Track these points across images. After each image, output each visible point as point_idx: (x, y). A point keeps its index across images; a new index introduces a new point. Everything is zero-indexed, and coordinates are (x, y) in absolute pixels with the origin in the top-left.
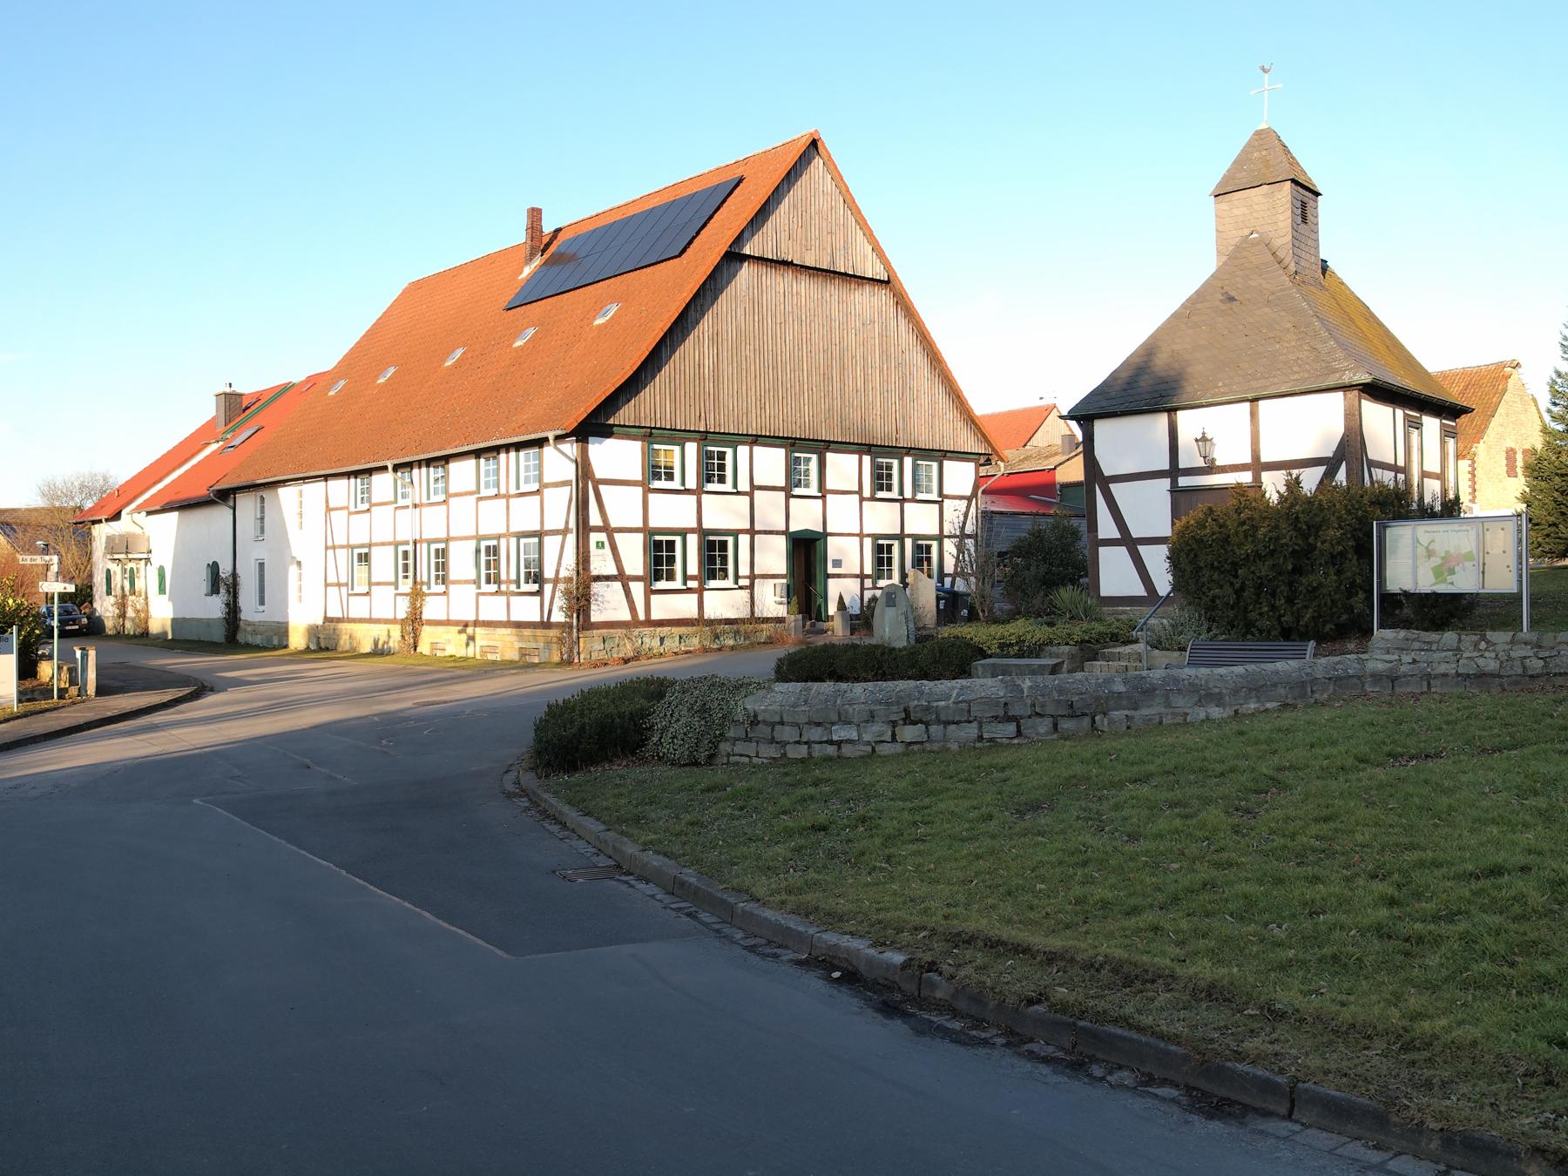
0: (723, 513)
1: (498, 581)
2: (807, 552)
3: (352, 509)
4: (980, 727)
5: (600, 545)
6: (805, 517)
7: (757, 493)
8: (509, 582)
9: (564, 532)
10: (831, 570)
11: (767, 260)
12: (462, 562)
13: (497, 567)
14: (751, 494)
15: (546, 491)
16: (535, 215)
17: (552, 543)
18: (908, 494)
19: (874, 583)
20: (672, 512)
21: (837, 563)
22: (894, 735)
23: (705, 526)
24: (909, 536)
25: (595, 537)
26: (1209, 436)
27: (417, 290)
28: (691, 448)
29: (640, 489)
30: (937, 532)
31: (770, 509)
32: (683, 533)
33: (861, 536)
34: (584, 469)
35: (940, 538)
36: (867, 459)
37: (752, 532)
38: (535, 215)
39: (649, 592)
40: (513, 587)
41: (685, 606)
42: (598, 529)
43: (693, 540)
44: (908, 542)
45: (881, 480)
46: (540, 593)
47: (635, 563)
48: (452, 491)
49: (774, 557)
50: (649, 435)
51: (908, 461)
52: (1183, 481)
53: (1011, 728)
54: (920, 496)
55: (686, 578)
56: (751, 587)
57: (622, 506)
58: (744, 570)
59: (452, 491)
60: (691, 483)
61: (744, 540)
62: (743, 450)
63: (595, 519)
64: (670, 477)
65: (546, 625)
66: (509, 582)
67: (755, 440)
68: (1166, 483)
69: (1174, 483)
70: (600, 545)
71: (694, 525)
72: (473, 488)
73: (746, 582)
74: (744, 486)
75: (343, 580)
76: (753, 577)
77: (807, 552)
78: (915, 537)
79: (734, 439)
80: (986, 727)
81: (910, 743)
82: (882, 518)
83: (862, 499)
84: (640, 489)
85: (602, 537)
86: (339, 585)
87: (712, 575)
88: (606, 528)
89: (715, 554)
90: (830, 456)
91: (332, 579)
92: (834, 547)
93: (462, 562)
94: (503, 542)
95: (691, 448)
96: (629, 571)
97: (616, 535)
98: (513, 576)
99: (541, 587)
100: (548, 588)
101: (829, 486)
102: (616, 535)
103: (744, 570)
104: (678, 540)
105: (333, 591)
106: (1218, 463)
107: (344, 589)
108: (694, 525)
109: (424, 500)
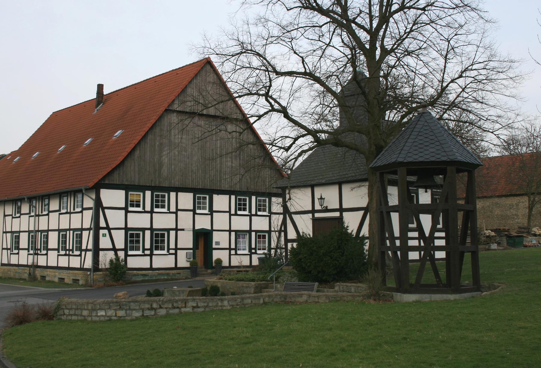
0: (163, 221)
1: (66, 250)
2: (203, 237)
3: (14, 216)
4: (143, 311)
5: (104, 235)
6: (203, 223)
7: (179, 212)
8: (69, 250)
9: (89, 229)
10: (214, 246)
11: (187, 113)
12: (53, 240)
13: (66, 243)
14: (176, 213)
15: (84, 212)
16: (100, 87)
17: (85, 234)
18: (253, 212)
19: (236, 252)
20: (139, 220)
21: (218, 243)
22: (116, 314)
23: (154, 227)
24: (254, 231)
25: (102, 232)
26: (323, 197)
27: (55, 115)
28: (148, 194)
29: (123, 211)
30: (268, 229)
31: (185, 220)
32: (143, 230)
33: (230, 231)
34: (98, 203)
35: (269, 232)
36: (233, 197)
37: (176, 230)
38: (100, 87)
39: (126, 255)
40: (71, 253)
41: (143, 262)
42: (103, 228)
43: (148, 233)
44: (253, 234)
45: (241, 206)
46: (80, 255)
47: (120, 243)
48: (50, 210)
49: (186, 240)
50: (127, 188)
51: (254, 198)
52: (317, 215)
53: (153, 313)
54: (259, 213)
55: (144, 249)
56: (176, 254)
57: (116, 219)
58: (172, 245)
59: (50, 210)
60: (148, 208)
61: (172, 233)
62: (173, 195)
63: (102, 224)
64: (138, 206)
65: (81, 269)
66: (69, 250)
67: (177, 190)
68: (310, 215)
69: (313, 216)
70: (104, 235)
71: (149, 226)
72: (58, 209)
73: (173, 252)
74: (173, 209)
75: (9, 247)
76: (176, 249)
77: (203, 237)
78: (256, 232)
79: (169, 190)
80: (145, 312)
81: (121, 317)
82: (241, 223)
83: (231, 215)
84: (123, 211)
85: (106, 231)
86: (7, 249)
87: (157, 248)
88: (108, 228)
89: (159, 238)
90: (215, 196)
91: (5, 247)
92: (216, 237)
93: (53, 240)
94: (68, 232)
95: (148, 194)
96: (117, 247)
97: (112, 231)
98: (71, 248)
99: (81, 253)
100: (83, 253)
101: (215, 209)
102: (112, 231)
103: (172, 245)
104: (141, 233)
105: (5, 252)
106: (329, 208)
107: (9, 251)
108: (149, 226)
109: (40, 214)
